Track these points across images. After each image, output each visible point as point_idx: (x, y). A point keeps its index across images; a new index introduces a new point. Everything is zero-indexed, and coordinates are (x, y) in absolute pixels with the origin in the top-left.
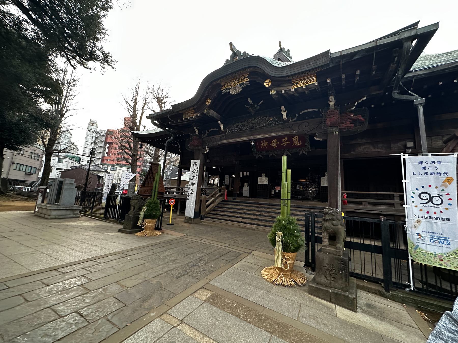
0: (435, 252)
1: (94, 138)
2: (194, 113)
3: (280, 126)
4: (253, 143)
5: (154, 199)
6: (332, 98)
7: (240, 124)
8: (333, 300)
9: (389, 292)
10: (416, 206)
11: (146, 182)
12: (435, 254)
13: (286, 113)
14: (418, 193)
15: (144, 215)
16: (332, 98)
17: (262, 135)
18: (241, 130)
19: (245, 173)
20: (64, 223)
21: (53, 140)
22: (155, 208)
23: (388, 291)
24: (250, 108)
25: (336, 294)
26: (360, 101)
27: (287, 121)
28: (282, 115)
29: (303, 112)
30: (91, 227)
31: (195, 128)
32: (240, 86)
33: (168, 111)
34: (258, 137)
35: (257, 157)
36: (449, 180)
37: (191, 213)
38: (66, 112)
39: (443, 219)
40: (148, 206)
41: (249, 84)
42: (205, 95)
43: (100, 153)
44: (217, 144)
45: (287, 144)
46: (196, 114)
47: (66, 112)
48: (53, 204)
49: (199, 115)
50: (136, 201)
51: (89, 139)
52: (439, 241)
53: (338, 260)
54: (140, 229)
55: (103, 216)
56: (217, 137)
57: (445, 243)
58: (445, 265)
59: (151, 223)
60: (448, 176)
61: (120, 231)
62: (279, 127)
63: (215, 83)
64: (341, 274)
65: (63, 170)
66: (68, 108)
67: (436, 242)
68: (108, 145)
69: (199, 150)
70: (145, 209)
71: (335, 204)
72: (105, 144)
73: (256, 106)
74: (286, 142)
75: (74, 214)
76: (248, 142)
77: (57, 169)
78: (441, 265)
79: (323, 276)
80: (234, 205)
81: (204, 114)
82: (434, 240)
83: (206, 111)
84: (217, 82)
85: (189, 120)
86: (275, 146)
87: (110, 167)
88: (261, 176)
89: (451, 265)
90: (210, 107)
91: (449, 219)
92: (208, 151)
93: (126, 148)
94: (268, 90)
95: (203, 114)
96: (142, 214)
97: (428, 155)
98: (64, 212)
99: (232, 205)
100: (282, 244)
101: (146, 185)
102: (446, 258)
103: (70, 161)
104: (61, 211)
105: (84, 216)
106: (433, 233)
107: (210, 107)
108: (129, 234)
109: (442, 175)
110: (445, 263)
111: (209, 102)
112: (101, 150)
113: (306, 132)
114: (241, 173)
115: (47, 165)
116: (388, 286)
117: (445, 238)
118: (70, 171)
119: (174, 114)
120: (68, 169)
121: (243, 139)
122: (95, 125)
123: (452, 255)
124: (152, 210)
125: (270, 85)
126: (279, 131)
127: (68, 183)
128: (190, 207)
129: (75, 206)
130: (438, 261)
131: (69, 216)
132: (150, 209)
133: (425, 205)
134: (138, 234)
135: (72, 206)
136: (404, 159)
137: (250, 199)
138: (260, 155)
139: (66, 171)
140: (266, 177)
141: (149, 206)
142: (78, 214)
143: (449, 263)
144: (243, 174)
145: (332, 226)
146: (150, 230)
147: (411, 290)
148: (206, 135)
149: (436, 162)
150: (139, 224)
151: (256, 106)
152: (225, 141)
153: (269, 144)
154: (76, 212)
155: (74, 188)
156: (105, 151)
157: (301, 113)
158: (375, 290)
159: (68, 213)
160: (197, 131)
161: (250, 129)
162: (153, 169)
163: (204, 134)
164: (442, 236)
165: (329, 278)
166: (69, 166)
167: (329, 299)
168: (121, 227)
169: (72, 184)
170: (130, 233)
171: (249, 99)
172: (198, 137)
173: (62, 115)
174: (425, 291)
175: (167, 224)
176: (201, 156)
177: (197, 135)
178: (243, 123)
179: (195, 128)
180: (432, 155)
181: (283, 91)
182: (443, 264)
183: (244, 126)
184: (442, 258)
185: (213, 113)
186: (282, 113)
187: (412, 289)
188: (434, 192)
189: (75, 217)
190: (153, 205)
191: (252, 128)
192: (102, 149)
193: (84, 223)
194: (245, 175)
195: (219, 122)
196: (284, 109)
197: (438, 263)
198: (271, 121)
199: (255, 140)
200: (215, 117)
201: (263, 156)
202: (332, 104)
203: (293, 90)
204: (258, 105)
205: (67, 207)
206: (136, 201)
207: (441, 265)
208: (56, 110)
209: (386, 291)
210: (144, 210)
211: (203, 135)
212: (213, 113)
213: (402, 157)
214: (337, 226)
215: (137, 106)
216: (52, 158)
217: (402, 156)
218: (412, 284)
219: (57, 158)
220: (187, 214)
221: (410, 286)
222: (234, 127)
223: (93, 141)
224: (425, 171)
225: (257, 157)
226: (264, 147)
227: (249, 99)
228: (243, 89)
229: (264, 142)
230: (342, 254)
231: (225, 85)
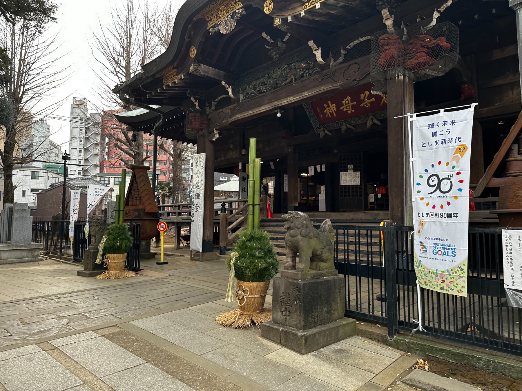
0: (437, 270)
1: (84, 130)
2: (177, 75)
3: (316, 76)
4: (279, 115)
5: (118, 223)
6: (385, 12)
7: (258, 82)
8: (282, 342)
9: (393, 337)
10: (422, 199)
11: (130, 199)
12: (437, 273)
13: (320, 51)
14: (426, 176)
15: (104, 247)
16: (385, 12)
17: (290, 99)
18: (260, 92)
19: (318, 167)
20: (21, 269)
21: (11, 144)
22: (119, 236)
23: (391, 334)
24: (272, 50)
25: (286, 333)
26: (442, 9)
27: (322, 67)
28: (315, 55)
29: (352, 44)
30: (47, 271)
31: (192, 98)
32: (232, 17)
33: (138, 78)
34: (285, 102)
35: (322, 134)
36: (461, 150)
37: (198, 244)
38: (23, 94)
39: (450, 215)
40: (109, 234)
41: (244, 13)
42: (186, 42)
43: (96, 155)
44: (227, 122)
45: (370, 103)
46: (179, 76)
47: (23, 94)
48: (6, 243)
49: (183, 77)
50: (97, 228)
51: (76, 132)
52: (443, 251)
53: (293, 285)
54: (101, 268)
55: (72, 257)
56: (227, 110)
57: (450, 254)
58: (448, 288)
59: (116, 260)
60: (461, 143)
61: (79, 274)
62: (315, 79)
63: (195, 19)
64: (296, 305)
65: (40, 191)
66: (26, 87)
67: (440, 253)
68: (107, 140)
69: (203, 136)
70: (105, 239)
71: (400, 209)
72: (103, 139)
73: (280, 44)
74: (368, 99)
75: (33, 256)
76: (271, 114)
77: (32, 190)
78: (442, 288)
79: (279, 310)
80: (277, 226)
81: (190, 74)
82: (437, 250)
83: (191, 69)
84: (199, 16)
85: (172, 87)
86: (350, 111)
87: (112, 179)
88: (346, 170)
89: (455, 288)
90: (198, 60)
91: (457, 214)
92: (217, 136)
93: (121, 142)
94: (270, 18)
95: (189, 74)
96: (101, 246)
97: (439, 112)
98: (18, 254)
99: (274, 226)
100: (235, 269)
101: (130, 203)
102: (449, 277)
103: (50, 175)
104: (15, 252)
105: (50, 258)
106: (437, 239)
107: (198, 60)
108: (89, 277)
109: (454, 141)
110: (447, 285)
111: (193, 52)
112: (97, 151)
113: (355, 83)
114: (324, 170)
115: (8, 186)
116: (393, 327)
117: (450, 246)
118: (51, 192)
119: (148, 80)
120: (48, 188)
121: (263, 109)
122: (82, 106)
123: (456, 272)
124: (114, 239)
125: (271, 9)
126: (315, 86)
127: (18, 210)
128: (196, 233)
129: (33, 243)
130: (440, 282)
131: (26, 259)
132: (112, 237)
133: (432, 195)
134: (101, 276)
135: (29, 244)
136: (412, 122)
137: (329, 213)
138: (326, 132)
139: (45, 191)
140: (355, 170)
141: (111, 234)
142: (38, 256)
143: (452, 285)
144: (315, 169)
145: (290, 238)
146: (116, 269)
147: (418, 331)
148: (213, 108)
149: (449, 122)
150: (98, 261)
151: (280, 44)
152: (239, 116)
153: (338, 107)
154: (36, 253)
155: (29, 216)
156: (104, 150)
157: (348, 47)
158: (378, 335)
159: (25, 254)
160: (197, 104)
161: (274, 89)
162: (137, 176)
163: (210, 106)
164: (446, 243)
165: (284, 313)
166: (49, 183)
167: (279, 341)
168: (81, 268)
169: (25, 210)
170: (90, 275)
171: (264, 35)
172: (198, 114)
173: (18, 100)
174: (477, 339)
175: (158, 264)
176: (208, 146)
177: (197, 111)
178: (262, 80)
179: (192, 98)
180: (445, 111)
181: (290, 19)
182: (445, 288)
183: (264, 84)
184: (444, 279)
185: (205, 70)
186: (314, 52)
187: (421, 330)
188: (443, 172)
189: (36, 260)
190: (117, 231)
191: (277, 88)
192: (99, 148)
193: (48, 266)
194: (319, 170)
195: (223, 83)
196: (315, 46)
197: (439, 287)
198: (303, 69)
199: (282, 108)
200: (211, 76)
201: (330, 131)
202: (389, 23)
203: (303, 13)
204: (284, 43)
205: (21, 246)
206: (97, 228)
207: (442, 288)
208: (9, 93)
209: (389, 336)
210: (104, 239)
211: (207, 109)
212: (205, 70)
213: (410, 119)
214: (296, 236)
215: (131, 65)
216: (14, 172)
217: (409, 117)
218: (420, 323)
219: (30, 173)
220: (192, 247)
221: (417, 325)
222: (250, 89)
223: (82, 136)
224: (435, 139)
225: (322, 134)
226: (332, 114)
227: (264, 35)
228: (238, 21)
229: (329, 106)
230: (300, 277)
231: (211, 20)
